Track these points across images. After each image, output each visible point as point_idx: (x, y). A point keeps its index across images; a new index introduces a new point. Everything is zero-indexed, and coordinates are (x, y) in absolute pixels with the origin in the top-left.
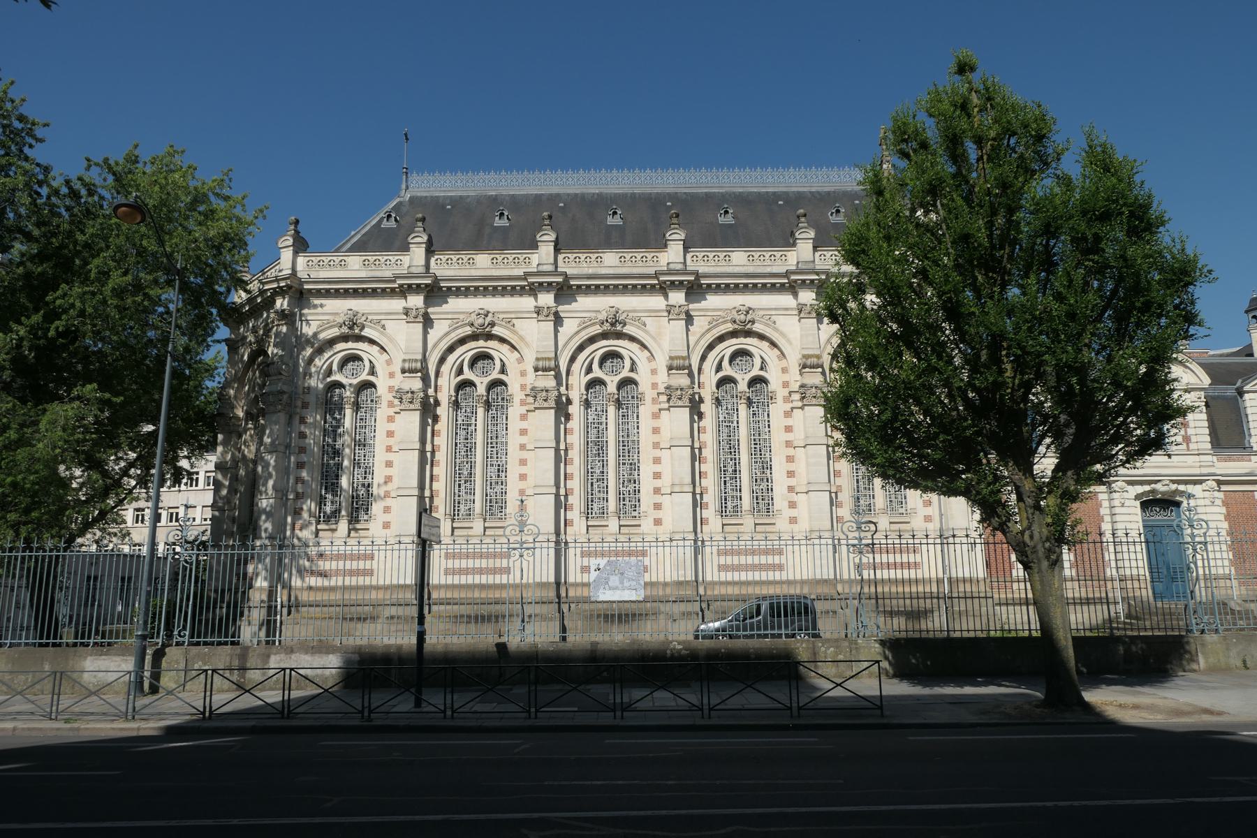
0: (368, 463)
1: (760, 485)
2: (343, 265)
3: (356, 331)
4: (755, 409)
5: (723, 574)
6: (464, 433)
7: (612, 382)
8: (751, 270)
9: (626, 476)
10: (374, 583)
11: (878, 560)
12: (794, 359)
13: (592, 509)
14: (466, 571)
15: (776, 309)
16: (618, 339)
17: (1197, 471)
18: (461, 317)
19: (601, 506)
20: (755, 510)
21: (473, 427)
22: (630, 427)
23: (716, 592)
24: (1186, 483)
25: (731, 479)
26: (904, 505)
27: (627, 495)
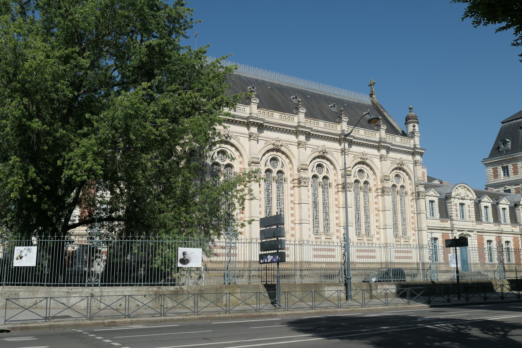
3: (228, 140)
7: (321, 177)
8: (366, 138)
12: (379, 175)
15: (373, 155)
16: (323, 159)
17: (472, 228)
18: (269, 140)
21: (270, 191)
23: (314, 266)
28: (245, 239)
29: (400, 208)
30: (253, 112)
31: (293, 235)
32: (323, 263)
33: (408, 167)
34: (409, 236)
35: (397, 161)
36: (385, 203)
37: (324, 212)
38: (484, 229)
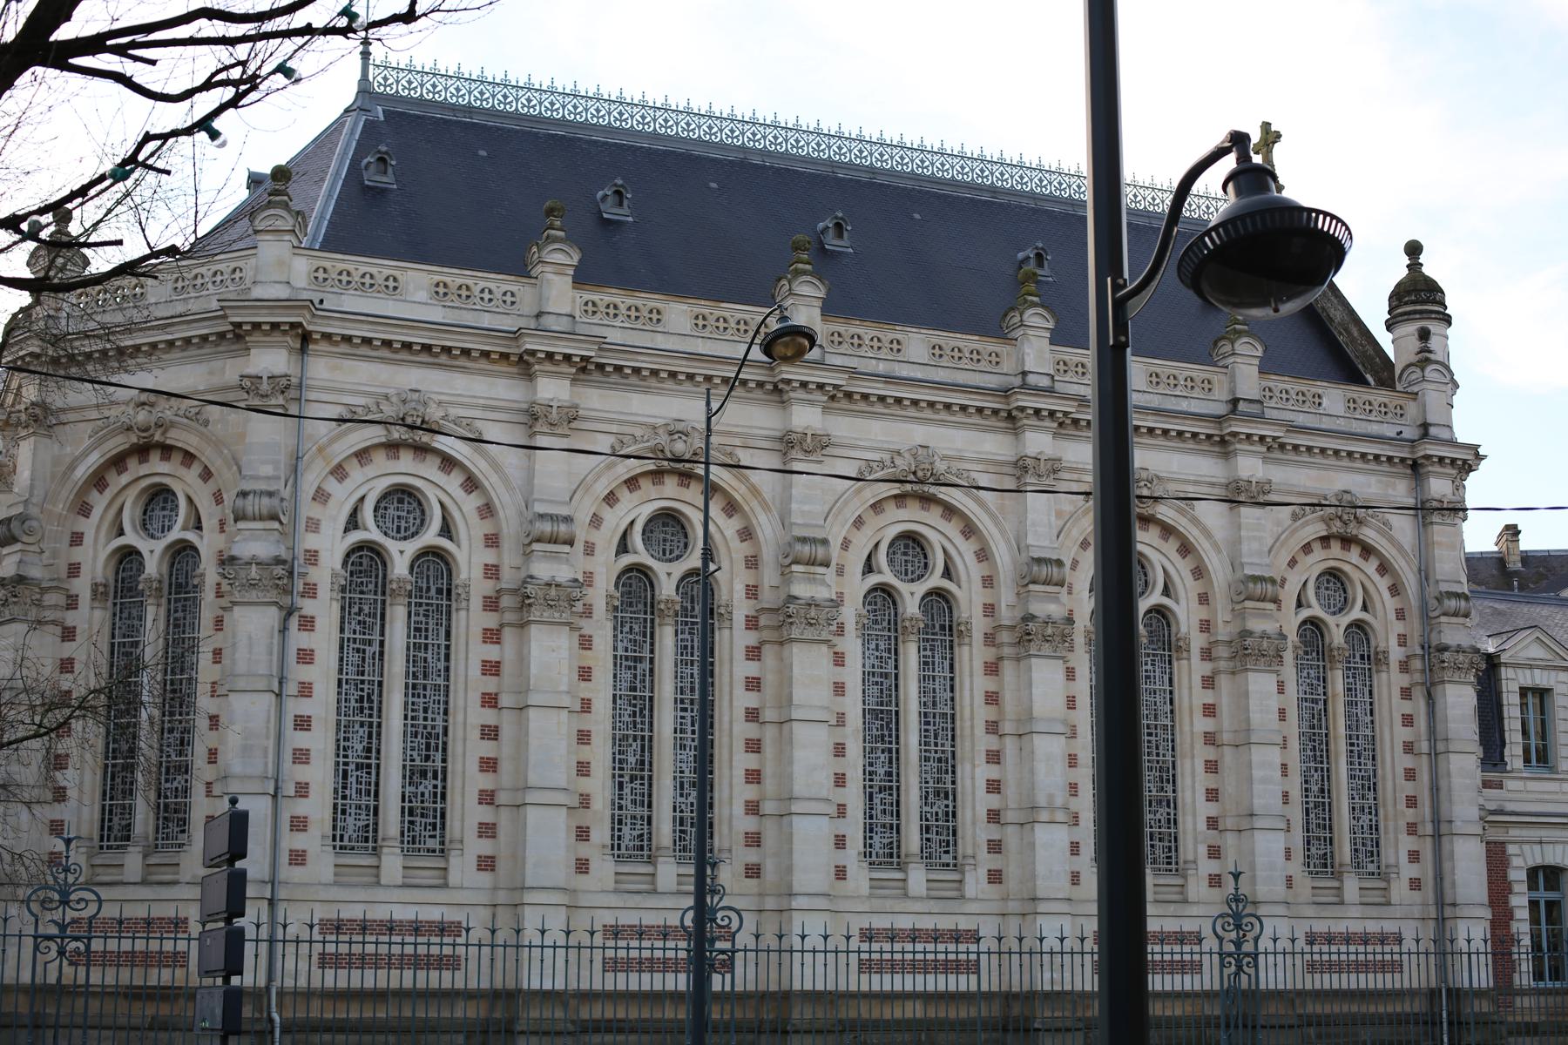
0: (433, 727)
1: (933, 804)
2: (392, 287)
4: (1149, 667)
9: (931, 784)
10: (459, 985)
13: (871, 846)
19: (886, 841)
20: (926, 855)
22: (937, 687)
25: (359, 767)
26: (951, 848)
29: (1342, 731)
32: (913, 996)
38: (1510, 807)
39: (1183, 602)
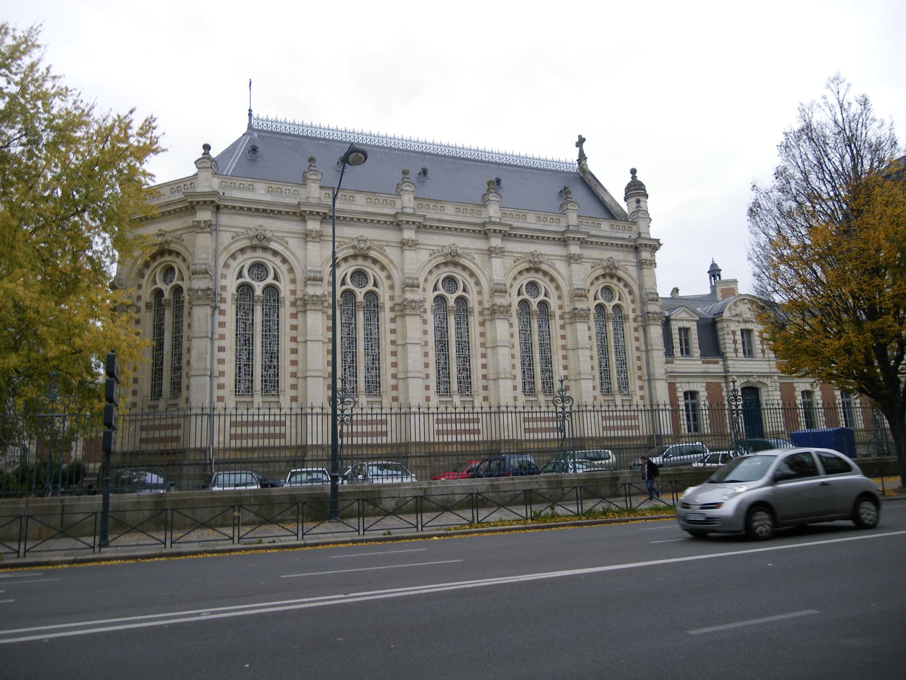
2: (251, 189)
5: (233, 442)
6: (347, 329)
11: (355, 430)
14: (537, 430)
18: (347, 241)
24: (764, 376)
25: (528, 370)
27: (370, 379)
28: (298, 408)
29: (613, 344)
30: (312, 195)
31: (395, 399)
33: (472, 260)
34: (633, 390)
35: (603, 262)
36: (577, 336)
37: (617, 360)
38: (676, 370)
39: (382, 288)
